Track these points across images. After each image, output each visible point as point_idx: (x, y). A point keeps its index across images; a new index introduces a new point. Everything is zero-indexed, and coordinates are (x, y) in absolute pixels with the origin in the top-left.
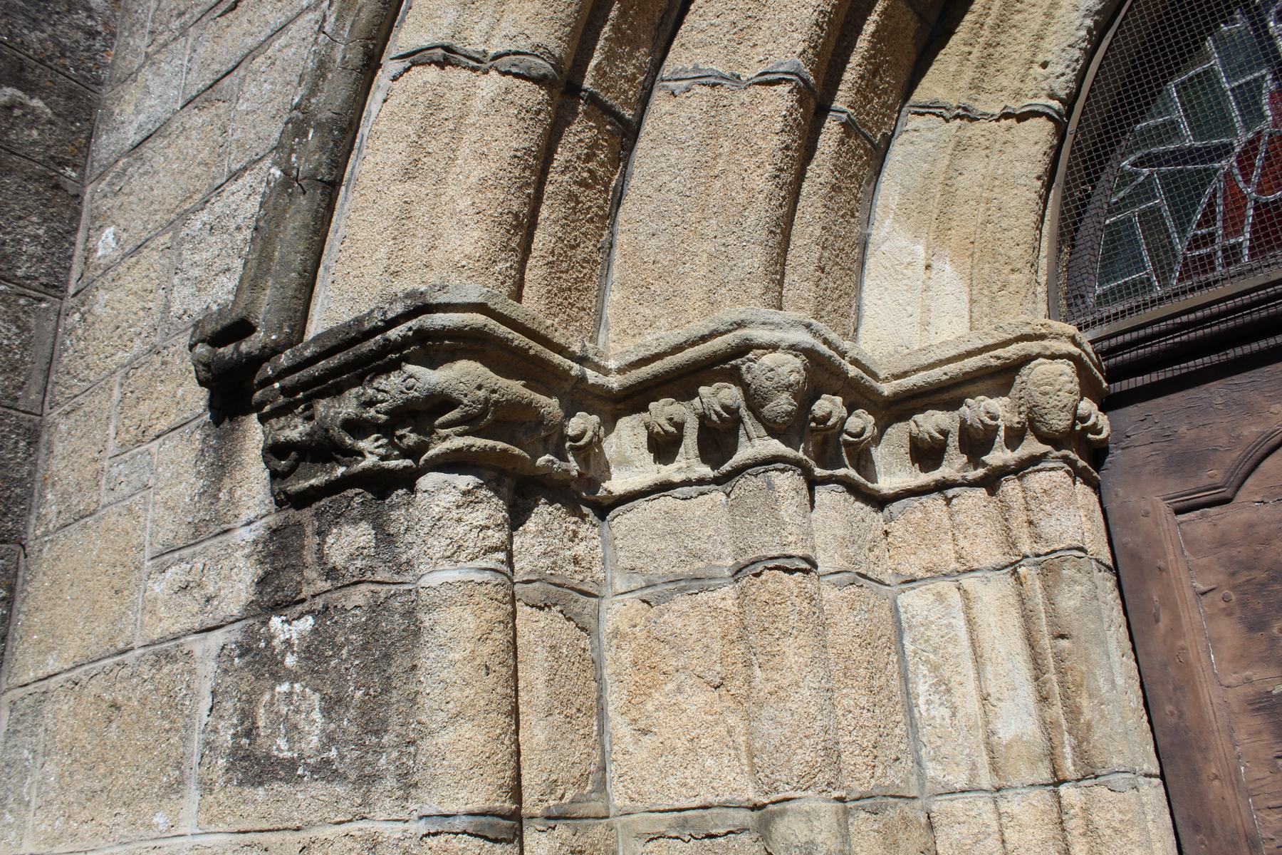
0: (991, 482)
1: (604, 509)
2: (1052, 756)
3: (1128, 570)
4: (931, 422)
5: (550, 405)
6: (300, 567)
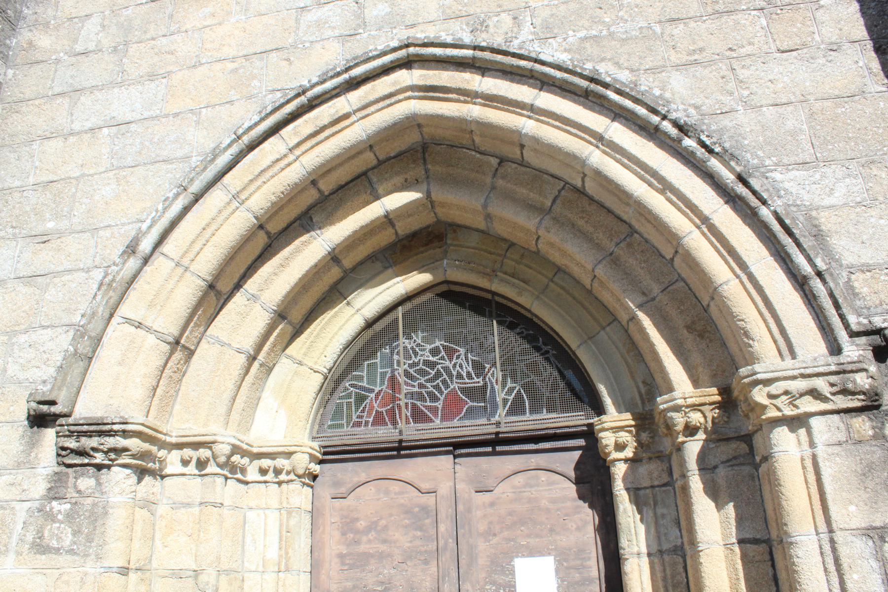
0: (280, 483)
1: (163, 477)
2: (279, 564)
3: (315, 514)
4: (266, 463)
5: (154, 449)
6: (67, 488)
